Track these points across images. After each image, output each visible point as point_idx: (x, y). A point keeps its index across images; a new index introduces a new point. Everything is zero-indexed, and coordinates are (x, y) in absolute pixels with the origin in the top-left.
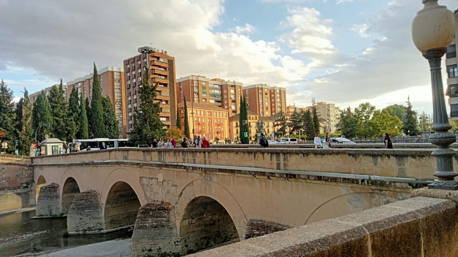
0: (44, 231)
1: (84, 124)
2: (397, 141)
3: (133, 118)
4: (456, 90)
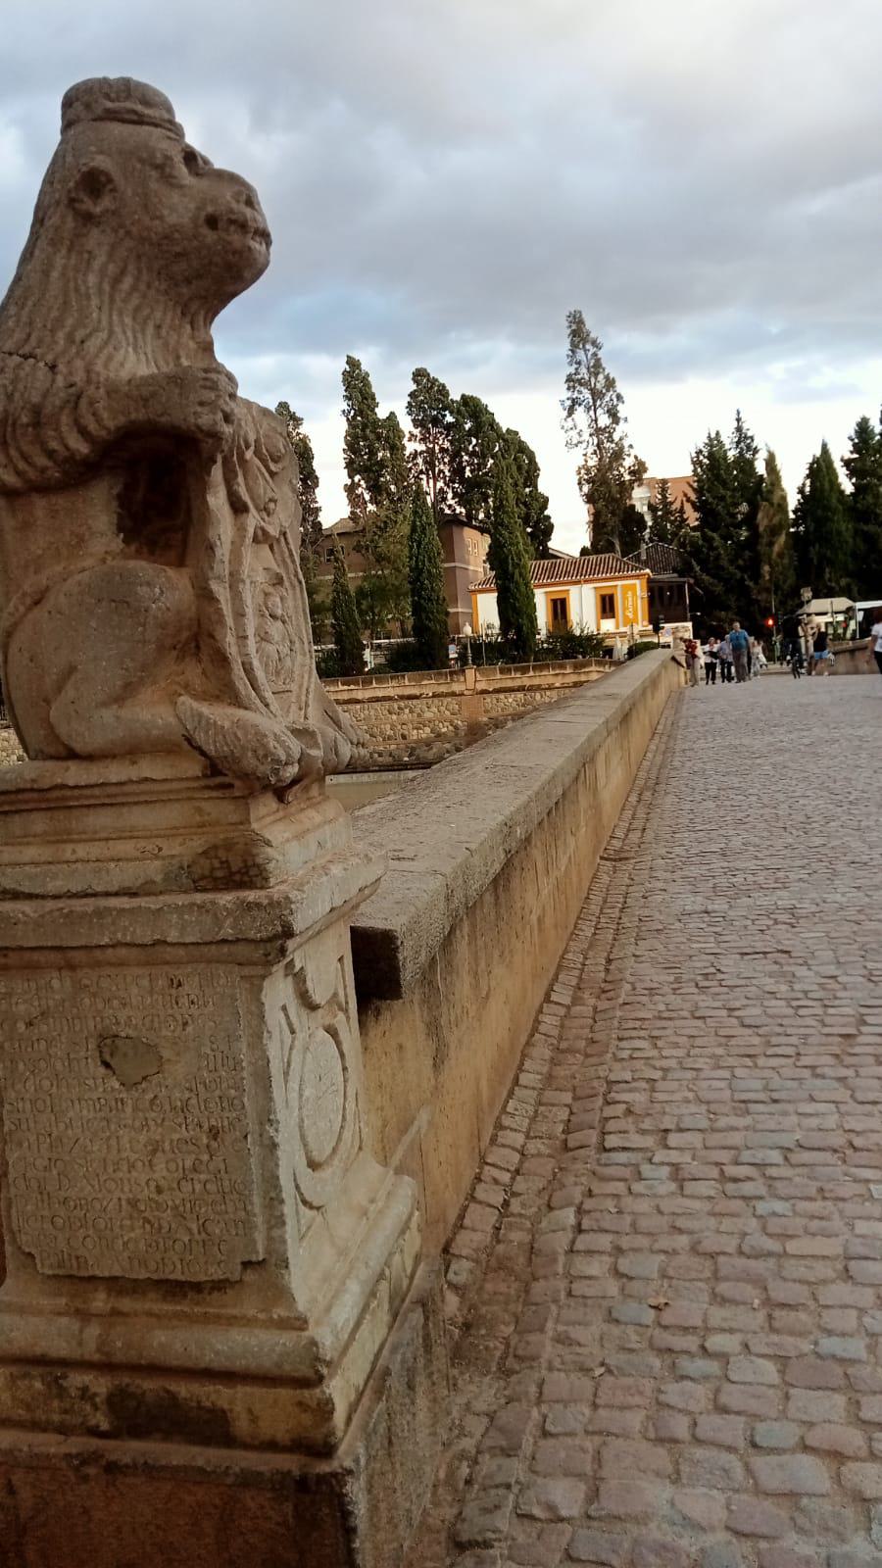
0: (182, 1311)
2: (276, 1233)
3: (807, 644)
4: (401, 958)
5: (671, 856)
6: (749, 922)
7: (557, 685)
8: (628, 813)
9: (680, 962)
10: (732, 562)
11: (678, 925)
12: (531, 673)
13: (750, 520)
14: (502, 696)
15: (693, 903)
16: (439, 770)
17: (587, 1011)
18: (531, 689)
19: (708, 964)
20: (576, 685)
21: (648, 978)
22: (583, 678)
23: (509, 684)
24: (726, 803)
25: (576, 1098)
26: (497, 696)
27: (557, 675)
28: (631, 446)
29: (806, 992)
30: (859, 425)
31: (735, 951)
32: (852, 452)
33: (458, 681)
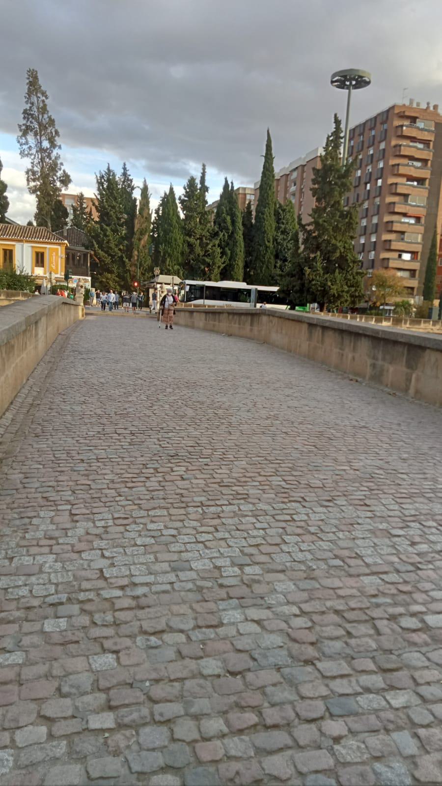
1: (236, 254)
10: (116, 246)
32: (185, 196)
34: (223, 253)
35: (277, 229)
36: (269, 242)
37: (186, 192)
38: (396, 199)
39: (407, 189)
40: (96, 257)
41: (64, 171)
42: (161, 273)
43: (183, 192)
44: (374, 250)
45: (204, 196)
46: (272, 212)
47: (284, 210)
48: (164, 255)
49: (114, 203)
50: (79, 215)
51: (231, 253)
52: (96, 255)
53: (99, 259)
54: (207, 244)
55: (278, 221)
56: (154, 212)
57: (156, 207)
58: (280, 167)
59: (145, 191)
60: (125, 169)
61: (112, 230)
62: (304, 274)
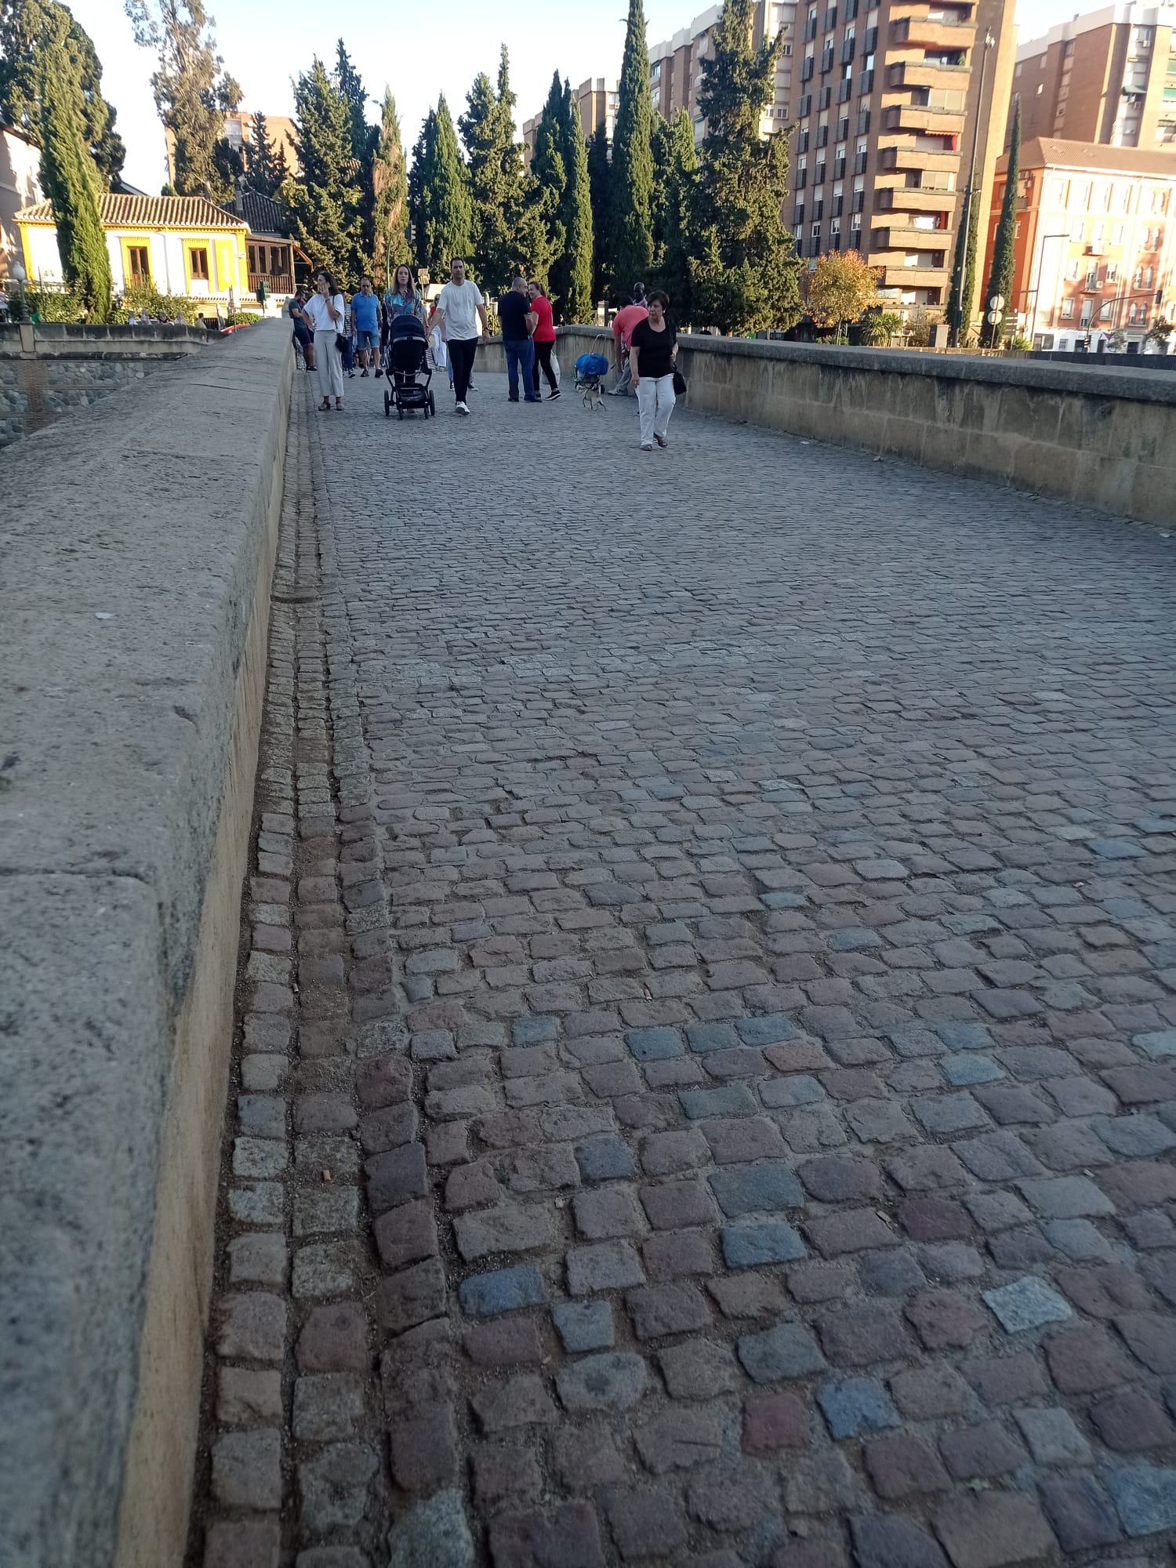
1: (578, 234)
5: (370, 597)
6: (520, 706)
7: (143, 355)
8: (290, 532)
9: (446, 779)
10: (342, 227)
11: (422, 713)
12: (109, 338)
13: (364, 179)
14: (71, 364)
15: (430, 673)
16: (21, 456)
17: (326, 885)
18: (110, 358)
19: (490, 782)
20: (167, 357)
21: (409, 813)
22: (175, 349)
23: (81, 349)
24: (415, 520)
25: (364, 1108)
26: (64, 363)
27: (141, 342)
28: (220, 59)
29: (654, 830)
30: (478, 82)
31: (520, 755)
32: (470, 116)
33: (11, 339)
34: (552, 233)
35: (658, 175)
36: (640, 204)
37: (473, 107)
38: (904, 99)
39: (924, 75)
40: (306, 252)
41: (227, 75)
42: (433, 281)
43: (466, 107)
44: (861, 210)
45: (507, 112)
46: (647, 141)
47: (670, 136)
48: (437, 243)
49: (332, 139)
50: (258, 163)
51: (567, 232)
52: (304, 248)
53: (310, 256)
54: (520, 215)
55: (659, 158)
56: (410, 151)
57: (416, 142)
58: (659, 37)
59: (388, 108)
60: (342, 53)
61: (331, 195)
62: (689, 271)
